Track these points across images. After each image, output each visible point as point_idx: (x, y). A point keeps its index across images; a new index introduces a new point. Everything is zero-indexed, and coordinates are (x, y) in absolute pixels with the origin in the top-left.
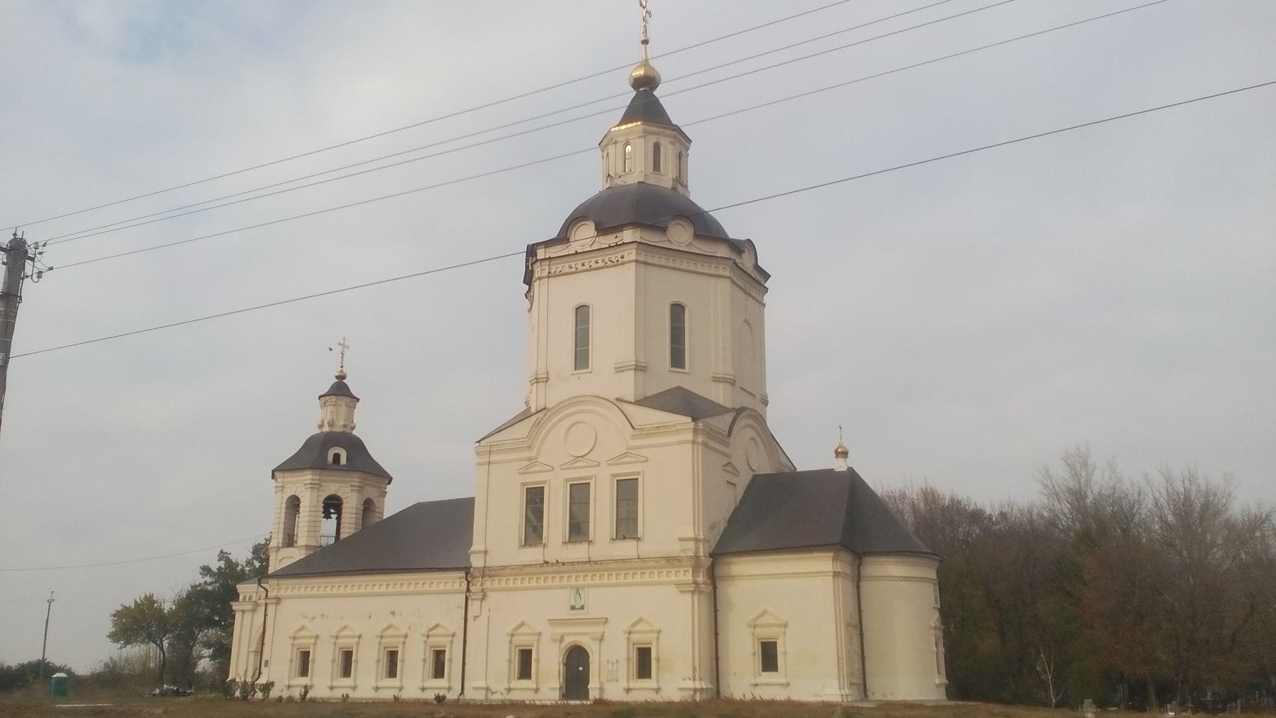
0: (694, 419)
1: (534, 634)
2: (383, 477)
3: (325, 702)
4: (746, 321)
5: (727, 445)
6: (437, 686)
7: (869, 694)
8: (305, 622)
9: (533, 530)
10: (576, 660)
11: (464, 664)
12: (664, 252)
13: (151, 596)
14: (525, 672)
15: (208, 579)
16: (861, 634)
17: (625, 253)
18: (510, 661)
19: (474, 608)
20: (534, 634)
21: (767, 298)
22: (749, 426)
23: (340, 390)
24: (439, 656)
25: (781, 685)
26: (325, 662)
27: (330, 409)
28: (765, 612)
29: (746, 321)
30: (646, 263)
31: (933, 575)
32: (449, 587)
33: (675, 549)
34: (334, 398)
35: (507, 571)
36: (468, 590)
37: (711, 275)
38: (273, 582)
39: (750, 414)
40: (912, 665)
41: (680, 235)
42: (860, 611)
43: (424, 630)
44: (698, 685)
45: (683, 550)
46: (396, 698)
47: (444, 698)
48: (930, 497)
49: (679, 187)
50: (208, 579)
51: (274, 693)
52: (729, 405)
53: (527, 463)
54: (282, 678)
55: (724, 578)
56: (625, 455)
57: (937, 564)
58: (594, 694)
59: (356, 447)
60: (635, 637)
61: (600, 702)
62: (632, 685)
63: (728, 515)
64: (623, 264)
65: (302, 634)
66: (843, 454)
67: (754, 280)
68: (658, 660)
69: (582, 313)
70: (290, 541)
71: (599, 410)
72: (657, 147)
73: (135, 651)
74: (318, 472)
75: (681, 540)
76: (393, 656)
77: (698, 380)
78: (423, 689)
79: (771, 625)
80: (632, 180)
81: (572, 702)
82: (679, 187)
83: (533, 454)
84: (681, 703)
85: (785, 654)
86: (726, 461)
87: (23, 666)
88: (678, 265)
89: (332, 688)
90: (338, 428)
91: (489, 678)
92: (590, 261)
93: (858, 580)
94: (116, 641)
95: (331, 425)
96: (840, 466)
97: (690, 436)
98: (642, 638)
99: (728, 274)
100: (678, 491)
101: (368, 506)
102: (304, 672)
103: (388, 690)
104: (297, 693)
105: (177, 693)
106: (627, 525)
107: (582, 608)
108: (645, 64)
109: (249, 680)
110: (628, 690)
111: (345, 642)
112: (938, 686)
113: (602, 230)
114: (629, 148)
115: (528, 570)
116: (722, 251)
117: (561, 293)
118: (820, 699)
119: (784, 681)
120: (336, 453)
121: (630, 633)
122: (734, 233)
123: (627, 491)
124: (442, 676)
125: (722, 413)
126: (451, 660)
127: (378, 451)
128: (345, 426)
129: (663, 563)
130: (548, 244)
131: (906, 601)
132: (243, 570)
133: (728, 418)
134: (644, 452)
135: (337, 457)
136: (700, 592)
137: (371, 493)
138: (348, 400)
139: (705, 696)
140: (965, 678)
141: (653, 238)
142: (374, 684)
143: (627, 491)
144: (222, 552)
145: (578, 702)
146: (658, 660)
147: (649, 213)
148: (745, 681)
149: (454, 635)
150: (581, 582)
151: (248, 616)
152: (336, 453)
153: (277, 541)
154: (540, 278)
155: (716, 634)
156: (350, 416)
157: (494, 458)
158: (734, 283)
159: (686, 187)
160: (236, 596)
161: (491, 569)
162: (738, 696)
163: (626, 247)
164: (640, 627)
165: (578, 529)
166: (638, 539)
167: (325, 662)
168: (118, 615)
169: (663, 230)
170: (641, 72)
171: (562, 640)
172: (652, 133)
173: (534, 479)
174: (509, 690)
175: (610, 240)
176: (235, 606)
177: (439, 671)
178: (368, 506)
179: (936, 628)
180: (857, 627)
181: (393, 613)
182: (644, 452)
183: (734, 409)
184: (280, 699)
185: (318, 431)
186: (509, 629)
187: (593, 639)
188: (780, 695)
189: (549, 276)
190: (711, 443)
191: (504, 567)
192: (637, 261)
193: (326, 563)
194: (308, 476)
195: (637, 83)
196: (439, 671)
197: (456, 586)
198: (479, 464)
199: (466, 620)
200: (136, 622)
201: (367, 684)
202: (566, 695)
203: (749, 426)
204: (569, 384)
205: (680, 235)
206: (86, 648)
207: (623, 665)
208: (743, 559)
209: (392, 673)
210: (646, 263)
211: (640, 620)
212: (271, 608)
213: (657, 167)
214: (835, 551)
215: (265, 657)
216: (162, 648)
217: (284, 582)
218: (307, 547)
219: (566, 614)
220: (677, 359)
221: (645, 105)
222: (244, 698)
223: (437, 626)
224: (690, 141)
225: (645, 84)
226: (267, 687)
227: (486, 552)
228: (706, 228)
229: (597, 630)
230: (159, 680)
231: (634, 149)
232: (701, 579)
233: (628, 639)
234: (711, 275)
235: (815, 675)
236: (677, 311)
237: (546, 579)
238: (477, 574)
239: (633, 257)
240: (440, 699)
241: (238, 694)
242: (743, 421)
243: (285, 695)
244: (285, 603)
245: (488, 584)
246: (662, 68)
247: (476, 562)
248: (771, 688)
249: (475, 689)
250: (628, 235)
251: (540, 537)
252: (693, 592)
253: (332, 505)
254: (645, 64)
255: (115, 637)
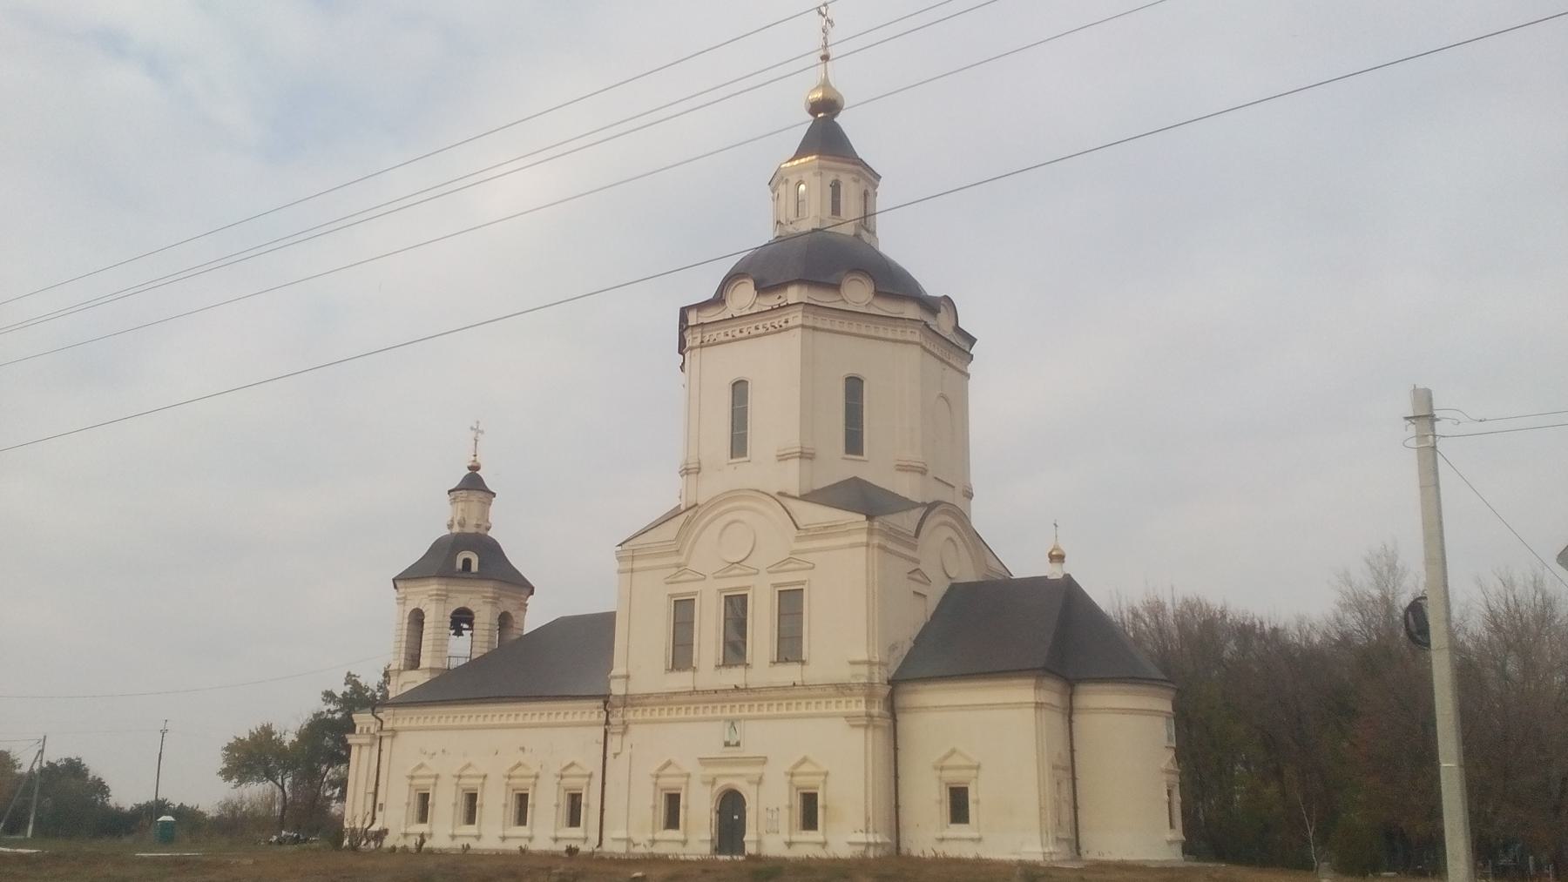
0: (869, 518)
1: (682, 776)
2: (521, 586)
3: (442, 854)
4: (943, 396)
5: (914, 547)
6: (574, 836)
7: (1083, 851)
8: (426, 760)
9: (681, 656)
10: (731, 807)
11: (602, 810)
12: (837, 314)
13: (269, 726)
14: (672, 821)
15: (332, 707)
16: (1074, 779)
17: (790, 317)
18: (654, 807)
19: (614, 743)
20: (682, 776)
21: (971, 368)
22: (945, 524)
23: (473, 483)
24: (575, 801)
25: (972, 840)
26: (446, 804)
27: (460, 505)
28: (953, 751)
29: (943, 396)
30: (815, 329)
31: (1166, 706)
32: (586, 718)
33: (844, 674)
34: (465, 493)
35: (652, 700)
36: (607, 722)
37: (896, 341)
38: (389, 711)
39: (948, 510)
40: (1137, 815)
41: (858, 293)
42: (1072, 751)
43: (557, 770)
44: (871, 839)
45: (854, 676)
46: (523, 851)
47: (577, 850)
48: (1191, 607)
49: (864, 233)
50: (332, 707)
51: (388, 842)
52: (917, 499)
53: (674, 570)
54: (398, 826)
55: (904, 710)
56: (788, 560)
57: (1173, 693)
58: (750, 849)
59: (490, 551)
60: (799, 780)
61: (756, 858)
62: (795, 838)
63: (915, 632)
64: (787, 329)
65: (420, 772)
66: (1056, 558)
67: (956, 347)
68: (825, 807)
69: (739, 389)
70: (413, 662)
71: (745, 503)
72: (836, 187)
73: (256, 791)
74: (444, 581)
75: (853, 663)
76: (523, 799)
77: (876, 469)
78: (556, 840)
79: (959, 768)
80: (805, 226)
81: (721, 858)
82: (864, 233)
83: (682, 560)
84: (846, 861)
85: (977, 802)
86: (913, 567)
87: (140, 807)
88: (881, 334)
89: (453, 837)
90: (470, 529)
91: (629, 827)
92: (749, 328)
93: (1069, 713)
94: (228, 778)
95: (462, 524)
96: (1054, 572)
97: (863, 538)
98: (805, 782)
99: (916, 337)
100: (853, 606)
101: (504, 621)
102: (423, 817)
103: (515, 839)
104: (411, 843)
105: (296, 840)
106: (789, 647)
107: (738, 744)
108: (825, 84)
109: (359, 826)
110: (790, 844)
111: (468, 783)
112: (1170, 843)
113: (762, 289)
114: (802, 187)
115: (675, 698)
116: (911, 311)
117: (724, 363)
118: (1015, 858)
119: (976, 835)
120: (468, 559)
121: (792, 775)
122: (932, 289)
123: (790, 603)
124: (578, 825)
125: (908, 509)
126: (587, 806)
127: (517, 557)
128: (478, 526)
129: (831, 690)
130: (700, 307)
131: (1131, 741)
132: (374, 696)
133: (917, 514)
134: (810, 557)
135: (467, 562)
136: (875, 727)
137: (508, 605)
138: (481, 494)
139: (879, 852)
140: (1209, 828)
141: (824, 298)
142: (501, 833)
143: (790, 603)
144: (349, 674)
145: (728, 858)
146: (825, 807)
147: (826, 267)
148: (930, 834)
149: (590, 776)
150: (737, 713)
151: (365, 751)
152: (468, 559)
153: (397, 662)
154: (691, 349)
155: (896, 777)
156: (484, 514)
157: (638, 564)
158: (924, 348)
159: (874, 233)
160: (352, 729)
161: (633, 697)
162: (916, 852)
163: (789, 310)
164: (805, 768)
165: (735, 649)
166: (803, 662)
167: (446, 804)
168: (230, 748)
169: (836, 287)
170: (819, 95)
171: (713, 783)
172: (830, 169)
173: (682, 589)
174: (653, 842)
175: (772, 301)
176: (351, 739)
177: (574, 820)
178: (504, 621)
179: (1168, 772)
180: (1068, 771)
181: (523, 749)
182: (810, 557)
183: (923, 504)
184: (394, 849)
185: (447, 532)
186: (654, 770)
187: (750, 782)
188: (968, 852)
189: (702, 345)
190: (891, 545)
191: (648, 696)
192: (803, 326)
193: (454, 689)
194: (433, 586)
195: (815, 108)
196: (574, 820)
197: (594, 718)
198: (620, 572)
199: (605, 758)
200: (250, 757)
201: (493, 834)
202: (720, 848)
203: (945, 524)
204: (724, 476)
205: (858, 293)
206: (204, 788)
207: (785, 813)
208: (929, 687)
209: (521, 819)
210: (815, 329)
211: (804, 760)
212: (386, 743)
213: (836, 209)
214: (1038, 677)
215: (379, 801)
216: (282, 788)
217: (402, 711)
218: (431, 669)
219: (717, 751)
220: (854, 443)
221: (825, 136)
222: (354, 848)
223: (572, 764)
224: (878, 177)
225: (826, 108)
226: (382, 833)
227: (627, 677)
228: (893, 283)
229: (755, 771)
230: (282, 823)
231: (808, 189)
232: (876, 710)
233: (791, 783)
234: (896, 341)
235: (1013, 830)
236: (854, 386)
237: (751, 706)
238: (618, 702)
239: (799, 321)
240: (572, 851)
241: (346, 842)
242: (935, 519)
243: (399, 845)
244: (401, 735)
245: (630, 716)
246: (845, 88)
247: (617, 688)
248: (960, 843)
249: (615, 840)
250: (793, 294)
251: (743, 655)
252: (866, 727)
253: (461, 620)
254: (825, 84)
255: (227, 774)
